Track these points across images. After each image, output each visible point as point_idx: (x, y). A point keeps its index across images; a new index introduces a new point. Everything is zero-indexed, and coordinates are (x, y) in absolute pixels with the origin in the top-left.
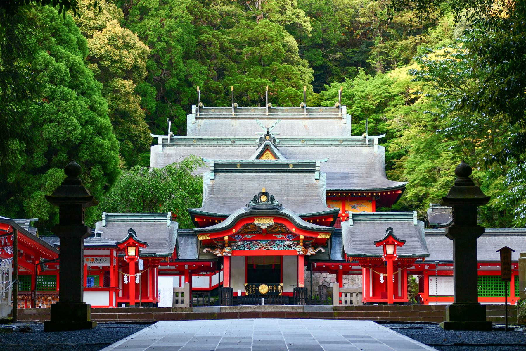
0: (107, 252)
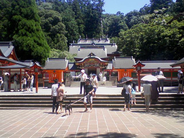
0: (19, 70)
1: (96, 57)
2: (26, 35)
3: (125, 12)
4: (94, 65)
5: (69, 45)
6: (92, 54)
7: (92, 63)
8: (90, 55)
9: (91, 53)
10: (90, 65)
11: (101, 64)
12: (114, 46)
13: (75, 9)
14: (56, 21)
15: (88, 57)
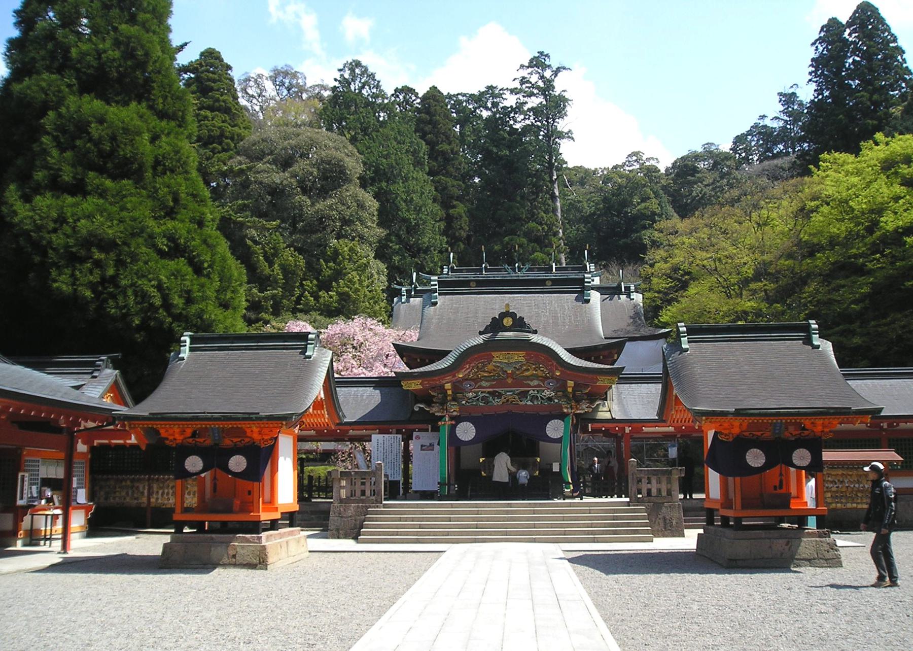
1: (535, 338)
2: (78, 189)
3: (664, 160)
4: (524, 395)
5: (392, 294)
6: (508, 322)
7: (510, 381)
8: (496, 325)
9: (503, 315)
10: (500, 396)
11: (571, 383)
12: (623, 297)
13: (428, 128)
14: (331, 178)
15: (480, 340)
